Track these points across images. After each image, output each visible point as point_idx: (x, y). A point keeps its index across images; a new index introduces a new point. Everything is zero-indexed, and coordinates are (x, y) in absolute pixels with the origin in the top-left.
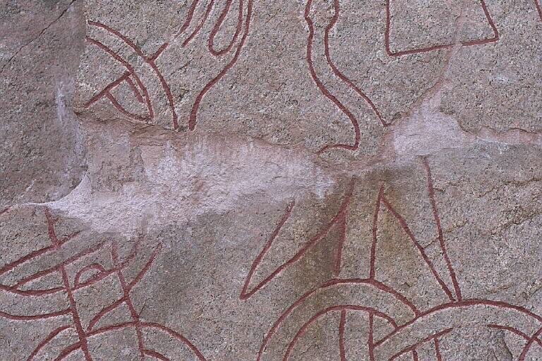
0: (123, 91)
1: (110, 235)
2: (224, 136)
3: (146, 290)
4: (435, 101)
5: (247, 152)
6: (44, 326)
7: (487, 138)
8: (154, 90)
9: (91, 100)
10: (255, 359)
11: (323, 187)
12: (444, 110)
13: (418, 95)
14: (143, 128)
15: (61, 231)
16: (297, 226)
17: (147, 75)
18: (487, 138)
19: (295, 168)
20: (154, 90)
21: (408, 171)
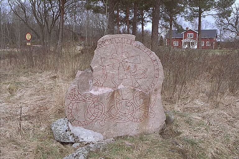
0: (97, 83)
1: (96, 95)
2: (105, 87)
3: (99, 99)
4: (122, 84)
5: (107, 88)
6: (91, 102)
7: (126, 87)
8: (99, 83)
9: (57, 36)
10: (53, 2)
11: (113, 91)
12: (123, 84)
13: (121, 83)
14: (98, 86)
15: (92, 95)
16: (111, 94)
17: (99, 82)
18: (126, 87)
19: (111, 89)
20: (99, 83)
21: (119, 89)
